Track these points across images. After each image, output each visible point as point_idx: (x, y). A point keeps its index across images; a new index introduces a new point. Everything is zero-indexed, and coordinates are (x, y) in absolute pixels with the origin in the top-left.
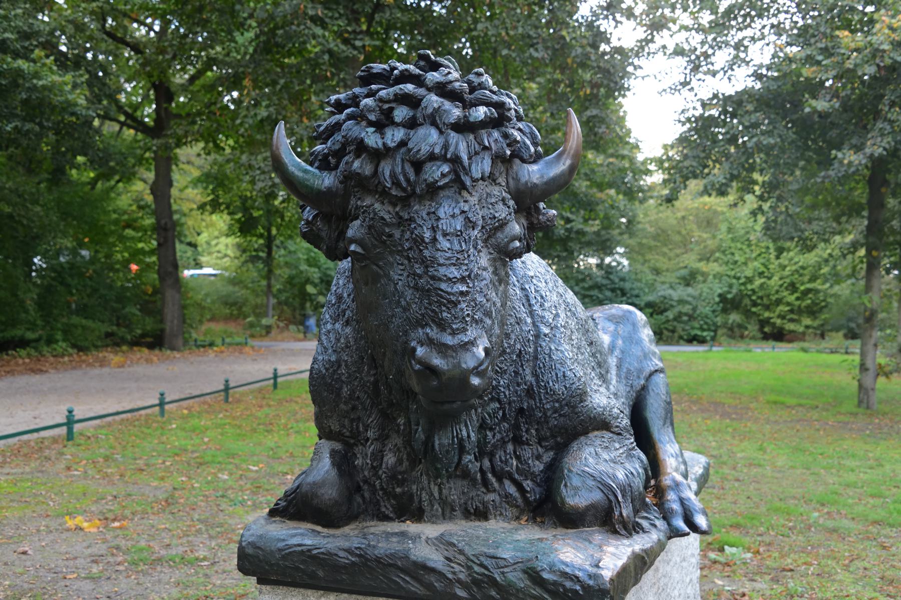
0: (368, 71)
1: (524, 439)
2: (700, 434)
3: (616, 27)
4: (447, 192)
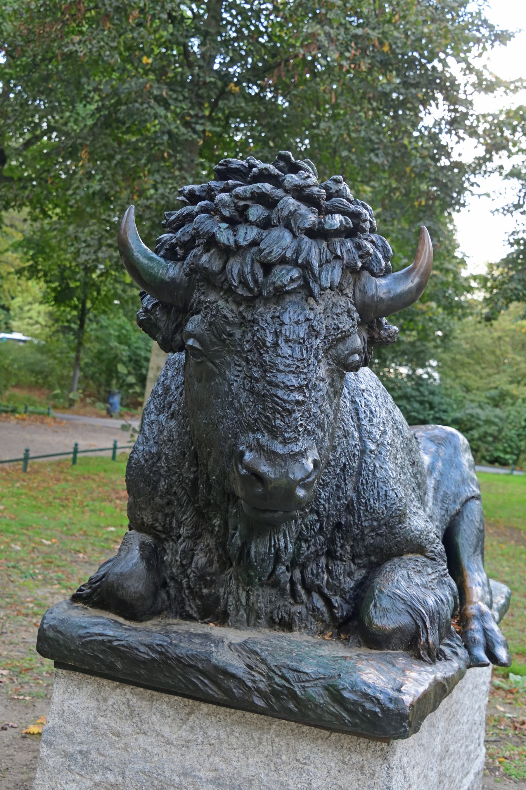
0: (226, 165)
1: (338, 554)
2: (494, 558)
3: (458, 142)
4: (293, 298)
